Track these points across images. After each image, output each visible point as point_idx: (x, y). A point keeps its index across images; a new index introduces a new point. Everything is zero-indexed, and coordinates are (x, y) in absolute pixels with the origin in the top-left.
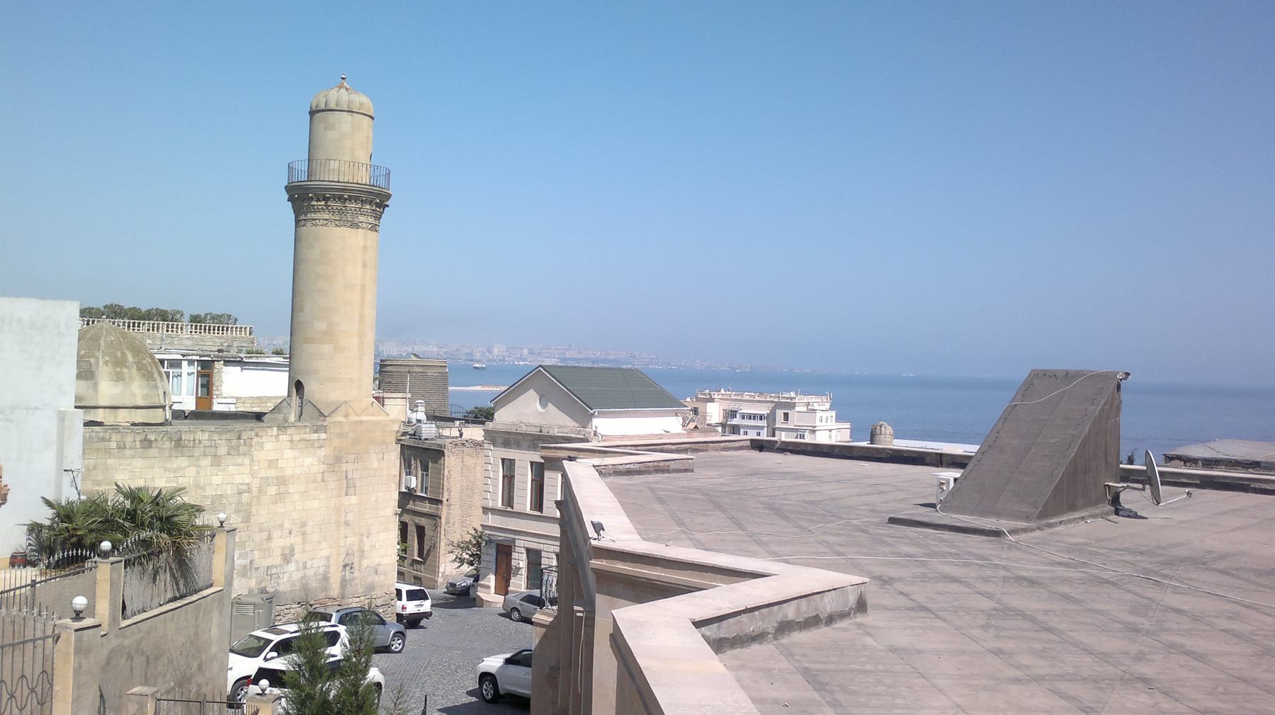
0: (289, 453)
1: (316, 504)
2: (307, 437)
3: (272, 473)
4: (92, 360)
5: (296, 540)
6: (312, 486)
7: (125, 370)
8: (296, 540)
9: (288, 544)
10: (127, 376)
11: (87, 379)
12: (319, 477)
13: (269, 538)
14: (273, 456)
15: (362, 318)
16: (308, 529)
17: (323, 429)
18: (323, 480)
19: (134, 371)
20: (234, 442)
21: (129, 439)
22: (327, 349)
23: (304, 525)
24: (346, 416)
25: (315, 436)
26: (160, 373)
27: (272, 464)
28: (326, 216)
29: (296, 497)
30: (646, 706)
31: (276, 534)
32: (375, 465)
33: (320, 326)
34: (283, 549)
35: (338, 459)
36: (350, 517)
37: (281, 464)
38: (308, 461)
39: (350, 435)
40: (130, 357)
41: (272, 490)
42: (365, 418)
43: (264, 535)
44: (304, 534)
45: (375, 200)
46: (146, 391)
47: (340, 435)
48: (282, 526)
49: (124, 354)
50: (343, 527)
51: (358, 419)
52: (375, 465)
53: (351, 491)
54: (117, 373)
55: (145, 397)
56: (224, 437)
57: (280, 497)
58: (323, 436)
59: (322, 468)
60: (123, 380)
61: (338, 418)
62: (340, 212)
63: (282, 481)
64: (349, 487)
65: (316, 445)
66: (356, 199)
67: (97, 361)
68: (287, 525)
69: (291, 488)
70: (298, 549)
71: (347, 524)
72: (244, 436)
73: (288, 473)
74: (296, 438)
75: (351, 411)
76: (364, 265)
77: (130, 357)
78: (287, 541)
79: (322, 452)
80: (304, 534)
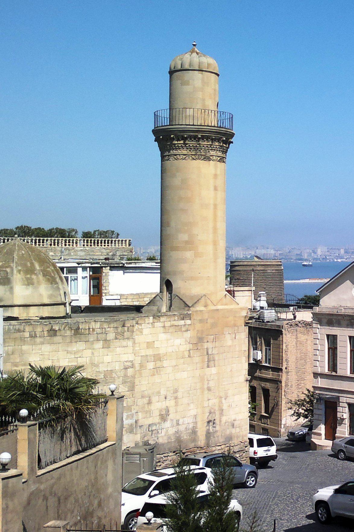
1: (185, 375)
2: (176, 323)
4: (8, 270)
5: (170, 403)
6: (182, 361)
7: (34, 277)
8: (170, 403)
9: (164, 407)
10: (35, 281)
12: (186, 354)
13: (150, 403)
14: (150, 339)
15: (215, 229)
17: (189, 317)
18: (189, 356)
19: (41, 277)
20: (120, 329)
22: (189, 254)
25: (182, 322)
27: (150, 345)
29: (169, 370)
31: (154, 399)
32: (229, 343)
36: (212, 384)
37: (157, 344)
38: (178, 342)
40: (37, 267)
41: (151, 365)
42: (220, 307)
43: (146, 400)
44: (176, 398)
46: (51, 292)
47: (201, 321)
48: (159, 393)
49: (32, 264)
50: (206, 392)
53: (212, 363)
54: (27, 279)
55: (50, 296)
57: (157, 370)
58: (188, 322)
60: (33, 284)
61: (200, 307)
62: (195, 148)
63: (158, 358)
64: (210, 361)
65: (183, 329)
66: (208, 138)
68: (163, 392)
69: (165, 363)
71: (209, 389)
72: (128, 324)
73: (162, 351)
74: (168, 324)
75: (209, 302)
76: (216, 189)
77: (37, 267)
78: (163, 405)
79: (188, 335)
80: (176, 398)
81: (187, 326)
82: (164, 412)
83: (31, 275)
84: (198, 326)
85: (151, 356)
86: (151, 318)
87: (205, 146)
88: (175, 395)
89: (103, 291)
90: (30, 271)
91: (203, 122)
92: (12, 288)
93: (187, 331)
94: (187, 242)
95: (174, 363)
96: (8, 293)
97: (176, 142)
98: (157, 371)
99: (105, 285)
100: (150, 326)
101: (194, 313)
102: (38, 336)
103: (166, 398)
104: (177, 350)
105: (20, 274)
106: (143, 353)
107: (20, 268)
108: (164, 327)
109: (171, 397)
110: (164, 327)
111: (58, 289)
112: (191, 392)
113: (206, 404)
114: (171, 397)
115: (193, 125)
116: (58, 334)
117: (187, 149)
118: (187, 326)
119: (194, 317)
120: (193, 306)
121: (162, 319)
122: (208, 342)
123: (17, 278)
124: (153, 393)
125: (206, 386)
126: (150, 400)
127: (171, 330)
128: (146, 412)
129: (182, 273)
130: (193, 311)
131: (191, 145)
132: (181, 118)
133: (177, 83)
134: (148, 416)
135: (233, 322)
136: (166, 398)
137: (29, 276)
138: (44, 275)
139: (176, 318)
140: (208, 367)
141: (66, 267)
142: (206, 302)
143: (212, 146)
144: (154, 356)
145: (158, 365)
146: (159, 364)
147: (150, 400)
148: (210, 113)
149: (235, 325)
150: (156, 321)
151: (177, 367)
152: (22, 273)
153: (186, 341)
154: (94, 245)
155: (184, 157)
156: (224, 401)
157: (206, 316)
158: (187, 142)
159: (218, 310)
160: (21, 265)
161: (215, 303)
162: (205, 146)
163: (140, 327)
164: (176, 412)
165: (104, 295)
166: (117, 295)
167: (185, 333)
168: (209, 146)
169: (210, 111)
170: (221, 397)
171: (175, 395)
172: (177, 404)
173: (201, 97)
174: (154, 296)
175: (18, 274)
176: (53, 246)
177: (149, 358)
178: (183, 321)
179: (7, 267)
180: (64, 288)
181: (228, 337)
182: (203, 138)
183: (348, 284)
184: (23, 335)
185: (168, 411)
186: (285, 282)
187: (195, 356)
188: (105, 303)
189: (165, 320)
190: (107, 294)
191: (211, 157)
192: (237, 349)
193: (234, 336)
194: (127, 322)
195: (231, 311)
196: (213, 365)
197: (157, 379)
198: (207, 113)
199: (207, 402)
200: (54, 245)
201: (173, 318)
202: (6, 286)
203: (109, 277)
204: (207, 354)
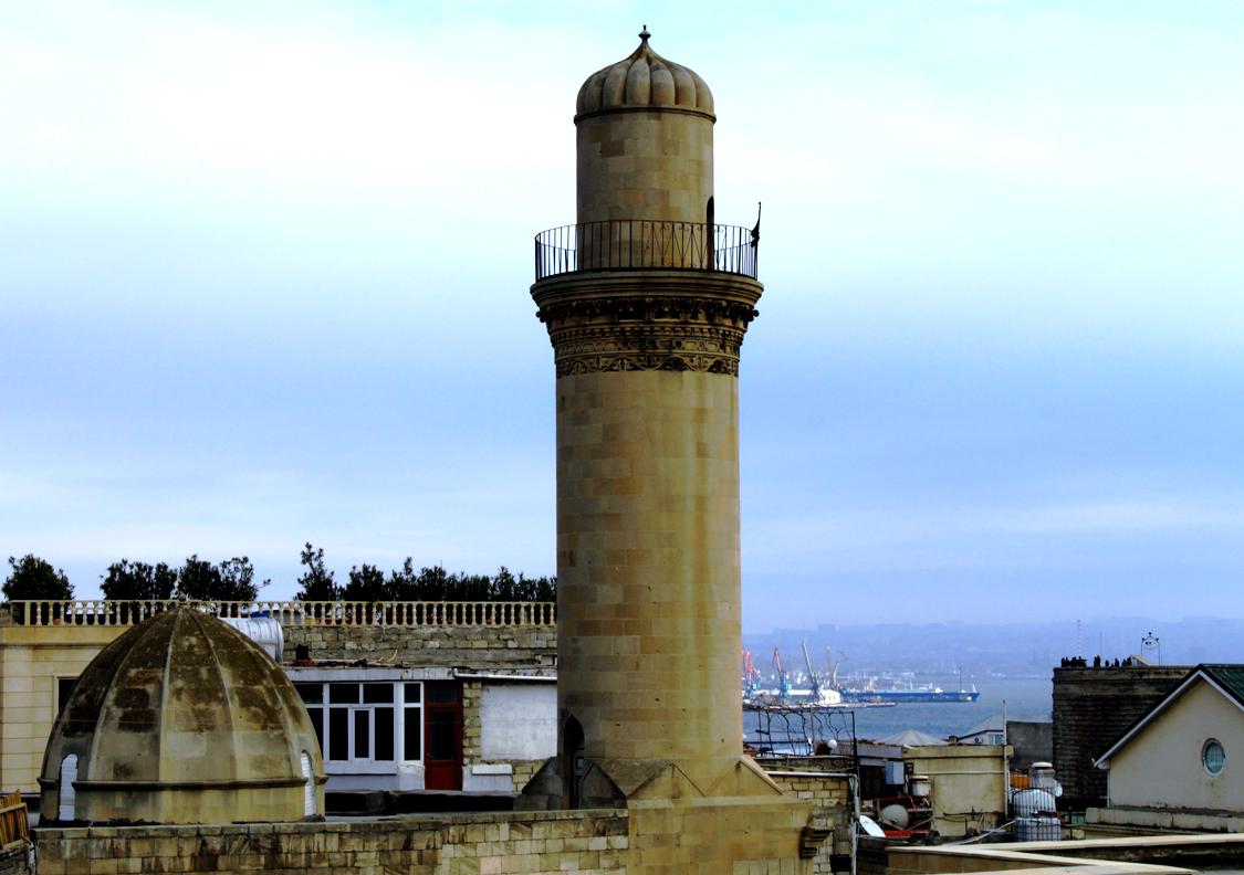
2: (581, 843)
4: (150, 689)
7: (215, 707)
10: (219, 721)
11: (137, 728)
17: (622, 827)
19: (234, 706)
20: (397, 857)
22: (625, 644)
24: (676, 796)
25: (600, 843)
26: (295, 713)
30: (732, 408)
39: (686, 840)
40: (226, 675)
42: (719, 800)
45: (632, 116)
46: (260, 751)
47: (659, 840)
49: (214, 672)
51: (700, 801)
54: (199, 714)
55: (259, 763)
56: (374, 845)
58: (620, 842)
60: (211, 728)
61: (654, 800)
67: (161, 689)
72: (420, 843)
77: (226, 675)
81: (616, 854)
83: (208, 703)
84: (652, 855)
86: (505, 827)
89: (466, 752)
90: (207, 691)
91: (657, 258)
92: (156, 739)
94: (620, 610)
96: (146, 753)
97: (587, 323)
99: (469, 732)
100: (501, 849)
101: (639, 817)
102: (166, 869)
105: (179, 699)
107: (179, 683)
108: (543, 854)
110: (543, 854)
111: (285, 741)
115: (631, 269)
116: (221, 862)
119: (639, 826)
120: (635, 795)
121: (539, 831)
123: (172, 709)
129: (607, 698)
130: (635, 811)
132: (606, 250)
133: (614, 149)
137: (202, 706)
138: (245, 703)
141: (427, 683)
142: (675, 785)
148: (678, 232)
149: (770, 855)
150: (517, 835)
152: (184, 696)
154: (469, 621)
155: (611, 360)
157: (675, 826)
159: (712, 809)
160: (184, 674)
161: (704, 790)
163: (471, 852)
165: (466, 761)
166: (506, 761)
169: (658, 226)
173: (656, 185)
174: (536, 769)
175: (174, 700)
176: (354, 623)
178: (604, 839)
179: (147, 681)
180: (301, 740)
184: (125, 866)
188: (470, 786)
190: (476, 760)
191: (686, 360)
194: (416, 836)
195: (754, 812)
198: (687, 234)
200: (359, 621)
202: (142, 734)
203: (481, 711)
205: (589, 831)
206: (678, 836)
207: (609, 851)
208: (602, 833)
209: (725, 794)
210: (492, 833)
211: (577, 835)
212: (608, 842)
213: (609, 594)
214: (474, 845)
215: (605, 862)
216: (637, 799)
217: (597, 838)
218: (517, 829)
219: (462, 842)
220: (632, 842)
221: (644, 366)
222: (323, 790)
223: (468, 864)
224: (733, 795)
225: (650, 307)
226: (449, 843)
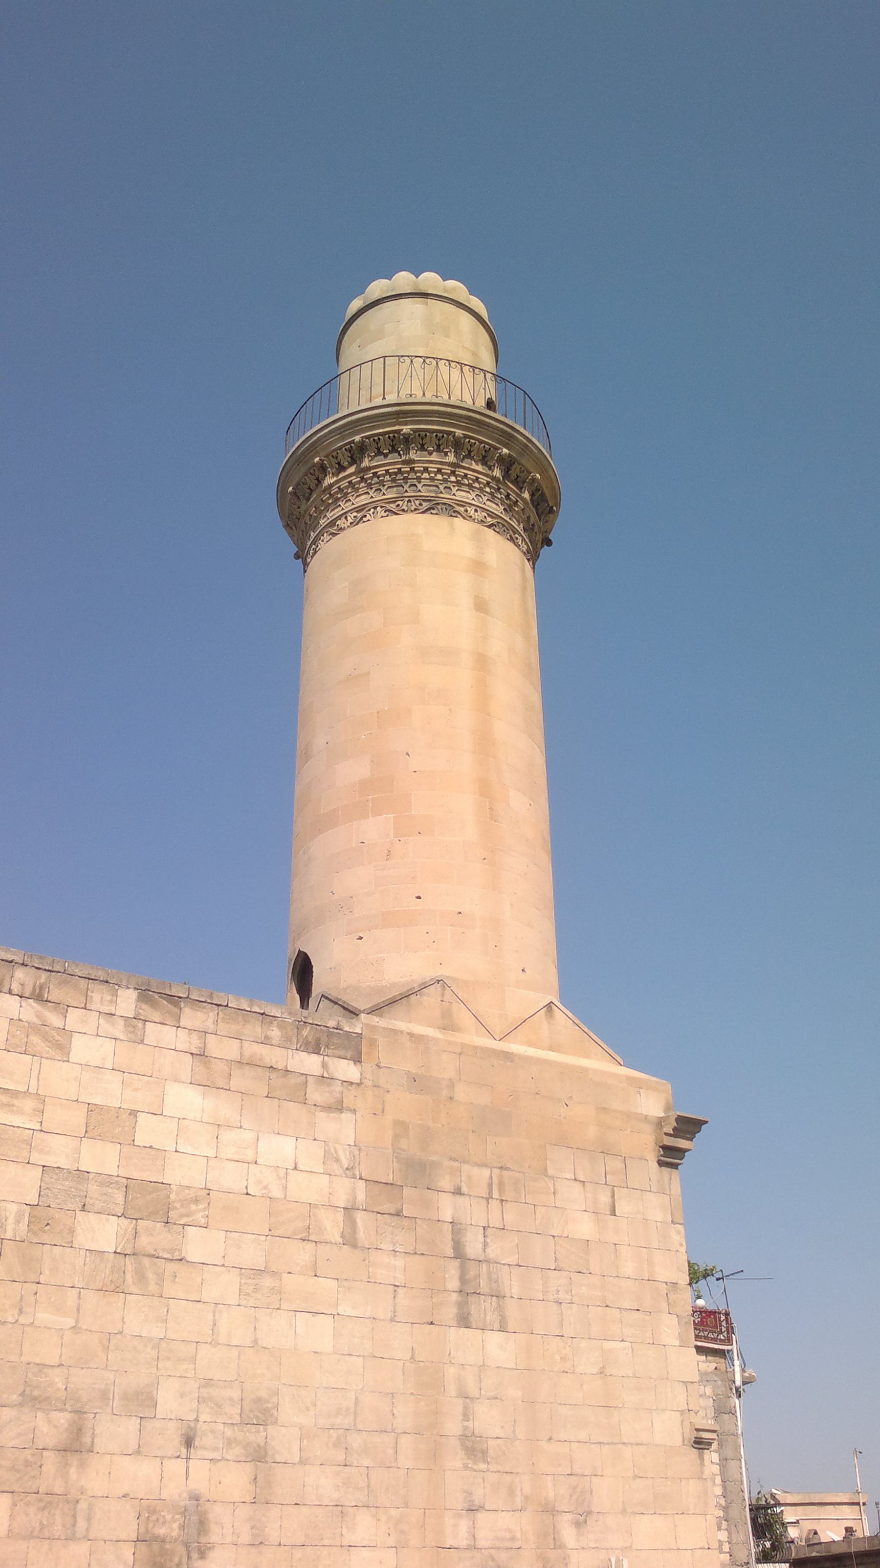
0: (185, 1099)
1: (317, 1334)
2: (274, 1056)
3: (100, 1158)
5: (224, 1481)
6: (302, 1254)
8: (224, 1481)
9: (175, 1490)
12: (332, 1226)
13: (76, 1446)
14: (111, 1093)
15: (484, 743)
16: (283, 1441)
18: (350, 1240)
21: (69, 1531)
22: (373, 829)
23: (260, 1414)
24: (449, 1025)
25: (311, 1063)
27: (101, 1123)
28: (363, 500)
29: (223, 1286)
31: (112, 1431)
32: (584, 1227)
33: (352, 771)
34: (148, 1511)
35: (418, 1172)
36: (488, 1420)
37: (147, 1131)
38: (280, 1149)
41: (103, 1233)
43: (51, 1427)
44: (259, 1456)
48: (142, 1402)
50: (455, 1460)
52: (584, 1227)
53: (483, 1309)
57: (137, 1268)
58: (346, 1070)
59: (343, 1190)
62: (397, 478)
63: (150, 1203)
64: (471, 1293)
65: (315, 1095)
66: (441, 442)
68: (170, 1401)
69: (198, 1245)
70: (227, 1525)
71: (474, 1448)
73: (182, 1174)
74: (223, 1048)
75: (462, 1016)
76: (481, 606)
78: (173, 1480)
79: (343, 1130)
80: (259, 1456)
81: (337, 1087)
82: (169, 1528)
85: (107, 1181)
87: (433, 468)
88: (256, 1436)
93: (338, 1107)
95: (252, 1253)
98: (140, 1276)
100: (118, 1029)
103: (189, 1442)
104: (276, 1193)
106: (59, 1153)
109: (230, 1443)
110: (201, 1055)
112: (356, 1441)
113: (458, 1532)
114: (230, 1443)
117: (370, 486)
118: (337, 1087)
121: (191, 1017)
122: (458, 1192)
124: (104, 1396)
125: (453, 1427)
126: (77, 1430)
127: (241, 1080)
128: (47, 1500)
131: (381, 471)
134: (58, 1529)
135: (592, 1132)
136: (189, 1442)
139: (275, 1033)
140: (464, 1321)
143: (461, 472)
144: (128, 1185)
145: (144, 1241)
146: (154, 1237)
147: (77, 1430)
150: (146, 1011)
151: (267, 1282)
153: (330, 1156)
156: (568, 1534)
157: (446, 1067)
158: (366, 463)
159: (508, 1056)
162: (433, 468)
163: (55, 1020)
164: (258, 1543)
167: (321, 1115)
168: (447, 470)
170: (549, 1510)
171: (256, 1436)
172: (261, 1497)
177: (93, 1188)
181: (573, 1195)
182: (419, 440)
183: (788, 1565)
185: (202, 1525)
186: (867, 1534)
187: (386, 1246)
189: (210, 1025)
192: (629, 1268)
193: (604, 1198)
196: (491, 1317)
197: (136, 1317)
199: (464, 1525)
201: (255, 1029)
204: (459, 1253)
205: (288, 1039)
206: (451, 1085)
207: (325, 1079)
208: (315, 1049)
209: (530, 1044)
210: (99, 997)
211: (266, 1041)
212: (324, 1066)
213: (87, 1440)
214: (62, 1008)
215: (315, 1095)
216: (381, 1016)
217: (304, 1055)
218: (153, 1004)
219: (38, 996)
220: (369, 1075)
221: (403, 510)
222: (695, 1434)
223: (45, 1038)
224: (544, 1049)
225: (407, 440)
226: (10, 992)
